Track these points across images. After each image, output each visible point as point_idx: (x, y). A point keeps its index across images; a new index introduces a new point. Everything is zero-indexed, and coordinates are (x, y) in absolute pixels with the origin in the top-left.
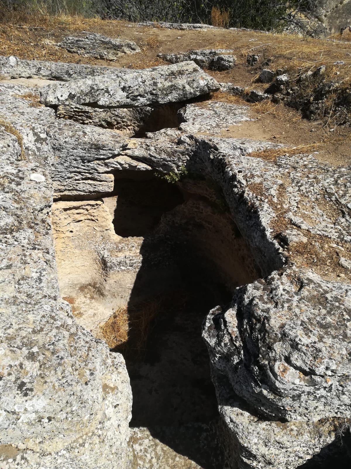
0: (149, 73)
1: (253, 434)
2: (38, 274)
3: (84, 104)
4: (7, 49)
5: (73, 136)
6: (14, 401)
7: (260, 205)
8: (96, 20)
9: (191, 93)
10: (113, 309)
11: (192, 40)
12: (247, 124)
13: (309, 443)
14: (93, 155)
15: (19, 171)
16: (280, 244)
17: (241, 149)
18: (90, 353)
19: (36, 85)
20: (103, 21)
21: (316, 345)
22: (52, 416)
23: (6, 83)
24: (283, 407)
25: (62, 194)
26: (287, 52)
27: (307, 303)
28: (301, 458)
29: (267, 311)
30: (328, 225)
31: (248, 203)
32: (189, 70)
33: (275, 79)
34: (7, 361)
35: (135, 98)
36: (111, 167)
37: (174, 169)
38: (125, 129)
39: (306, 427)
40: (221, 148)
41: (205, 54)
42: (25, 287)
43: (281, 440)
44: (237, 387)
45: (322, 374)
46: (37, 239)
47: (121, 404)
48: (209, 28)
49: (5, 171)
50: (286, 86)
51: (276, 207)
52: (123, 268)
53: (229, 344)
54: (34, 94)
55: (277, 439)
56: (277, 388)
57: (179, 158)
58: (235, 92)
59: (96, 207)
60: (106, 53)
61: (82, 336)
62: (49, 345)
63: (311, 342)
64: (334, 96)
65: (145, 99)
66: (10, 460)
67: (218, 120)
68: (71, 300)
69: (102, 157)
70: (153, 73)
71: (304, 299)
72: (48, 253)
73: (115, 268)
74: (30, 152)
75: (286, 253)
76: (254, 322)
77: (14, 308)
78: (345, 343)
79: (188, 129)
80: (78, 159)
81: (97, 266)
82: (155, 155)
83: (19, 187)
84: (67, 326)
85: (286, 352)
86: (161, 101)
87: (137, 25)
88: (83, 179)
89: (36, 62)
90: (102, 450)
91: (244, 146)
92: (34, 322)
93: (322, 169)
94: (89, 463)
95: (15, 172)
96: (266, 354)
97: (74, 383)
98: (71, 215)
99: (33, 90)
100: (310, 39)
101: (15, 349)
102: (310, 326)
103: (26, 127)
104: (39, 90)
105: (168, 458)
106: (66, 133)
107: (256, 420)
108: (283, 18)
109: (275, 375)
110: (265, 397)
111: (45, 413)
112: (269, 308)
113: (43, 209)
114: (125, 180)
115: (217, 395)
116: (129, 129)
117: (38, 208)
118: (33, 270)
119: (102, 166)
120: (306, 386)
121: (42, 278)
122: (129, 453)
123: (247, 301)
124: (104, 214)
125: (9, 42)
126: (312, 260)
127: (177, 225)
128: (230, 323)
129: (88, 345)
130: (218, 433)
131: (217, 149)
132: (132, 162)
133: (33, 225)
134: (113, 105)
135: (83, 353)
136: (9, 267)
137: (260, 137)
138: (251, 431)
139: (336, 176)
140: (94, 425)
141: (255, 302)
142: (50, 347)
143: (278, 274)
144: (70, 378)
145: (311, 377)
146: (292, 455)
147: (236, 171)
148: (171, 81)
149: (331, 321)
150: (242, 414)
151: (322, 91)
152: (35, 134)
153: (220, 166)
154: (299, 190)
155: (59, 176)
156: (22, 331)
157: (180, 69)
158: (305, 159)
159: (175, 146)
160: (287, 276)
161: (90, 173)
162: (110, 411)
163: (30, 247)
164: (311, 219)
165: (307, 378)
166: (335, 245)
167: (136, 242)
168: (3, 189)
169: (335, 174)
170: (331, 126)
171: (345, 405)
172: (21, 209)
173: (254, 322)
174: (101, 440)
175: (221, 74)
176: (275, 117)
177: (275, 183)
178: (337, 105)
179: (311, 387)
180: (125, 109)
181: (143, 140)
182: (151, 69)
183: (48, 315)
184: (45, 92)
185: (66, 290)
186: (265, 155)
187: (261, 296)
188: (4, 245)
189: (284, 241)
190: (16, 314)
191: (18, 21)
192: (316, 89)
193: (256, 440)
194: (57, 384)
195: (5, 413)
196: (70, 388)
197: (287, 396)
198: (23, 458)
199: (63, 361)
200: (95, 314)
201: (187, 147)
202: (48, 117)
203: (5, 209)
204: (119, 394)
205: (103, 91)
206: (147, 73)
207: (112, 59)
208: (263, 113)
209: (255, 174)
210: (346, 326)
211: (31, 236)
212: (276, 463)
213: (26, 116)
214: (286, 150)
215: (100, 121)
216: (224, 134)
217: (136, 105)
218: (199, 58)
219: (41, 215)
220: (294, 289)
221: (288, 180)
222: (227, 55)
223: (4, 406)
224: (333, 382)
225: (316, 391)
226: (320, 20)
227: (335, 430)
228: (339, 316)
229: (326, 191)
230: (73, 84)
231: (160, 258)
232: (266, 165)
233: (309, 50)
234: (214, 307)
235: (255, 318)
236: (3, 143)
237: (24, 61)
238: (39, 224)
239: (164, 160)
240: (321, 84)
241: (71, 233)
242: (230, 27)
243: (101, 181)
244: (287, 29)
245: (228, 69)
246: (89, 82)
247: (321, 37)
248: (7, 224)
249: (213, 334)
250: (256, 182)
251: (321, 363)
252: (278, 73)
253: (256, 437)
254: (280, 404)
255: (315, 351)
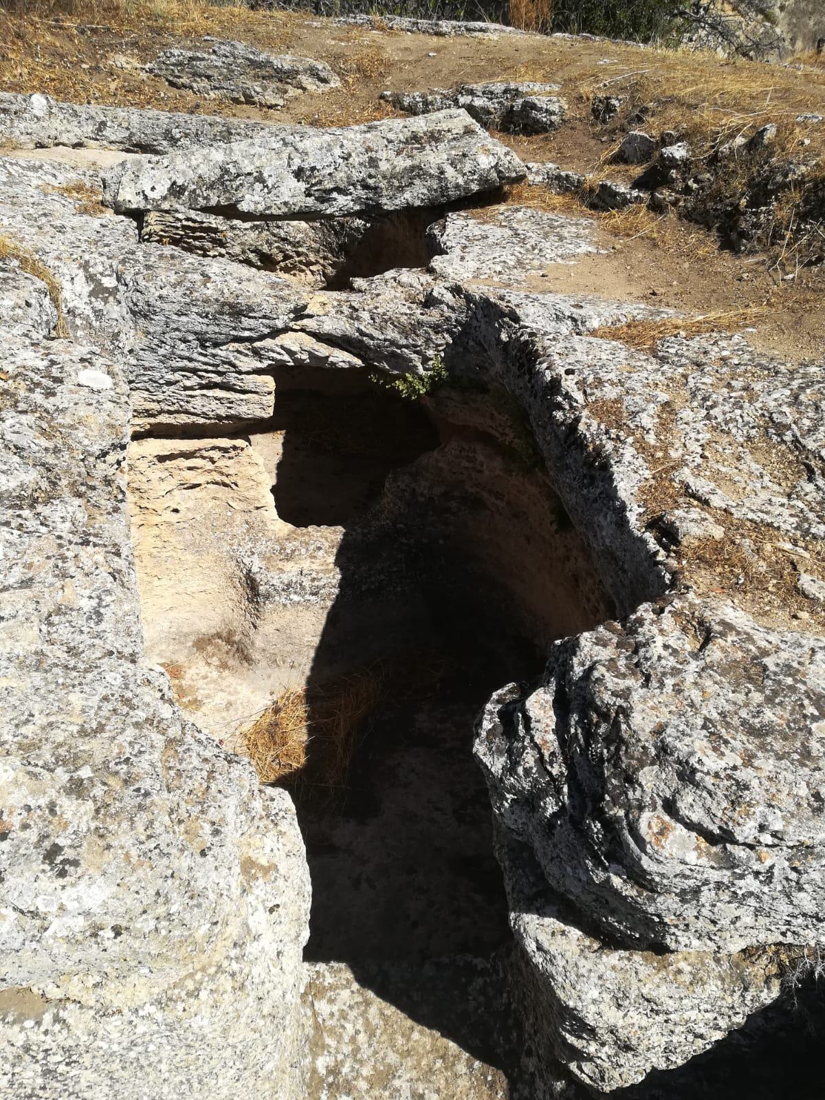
0: (358, 135)
1: (589, 978)
2: (94, 602)
3: (206, 210)
4: (26, 77)
5: (180, 283)
6: (33, 885)
7: (616, 450)
8: (236, 10)
9: (457, 186)
10: (272, 693)
11: (462, 61)
12: (589, 260)
13: (719, 1003)
14: (225, 330)
15: (53, 363)
16: (660, 542)
17: (574, 320)
18: (213, 786)
19: (94, 164)
20: (252, 13)
21: (738, 773)
22: (124, 924)
23: (23, 157)
24: (659, 916)
25: (152, 420)
26: (689, 90)
27: (718, 678)
28: (701, 1036)
29: (626, 694)
30: (774, 499)
31: (587, 446)
32: (454, 132)
33: (657, 154)
34: (18, 798)
35: (325, 197)
36: (269, 358)
37: (415, 366)
38: (303, 271)
39: (713, 964)
40: (527, 316)
41: (492, 93)
42: (63, 632)
43: (654, 994)
44: (551, 869)
45: (750, 841)
46: (92, 522)
47: (285, 904)
48: (502, 31)
49: (19, 364)
50: (684, 172)
51: (653, 456)
52: (296, 598)
53: (534, 770)
54: (88, 185)
55: (645, 991)
56: (645, 871)
57: (428, 340)
58: (563, 184)
59: (233, 453)
60: (259, 89)
61: (195, 747)
62: (116, 764)
63: (724, 765)
64: (796, 196)
65: (349, 197)
66: (29, 1024)
67: (522, 250)
68: (175, 671)
69: (247, 334)
70: (368, 135)
71: (711, 668)
72: (118, 554)
73: (277, 598)
74: (78, 321)
75: (673, 563)
76: (595, 720)
77: (37, 678)
78: (806, 770)
79: (450, 270)
80: (190, 338)
81: (236, 593)
82: (370, 330)
83: (51, 399)
84: (159, 722)
85: (667, 790)
86: (388, 204)
87: (334, 23)
88: (202, 387)
89: (94, 109)
90: (239, 1006)
91: (581, 312)
92: (83, 711)
93: (763, 368)
94: (210, 1036)
95: (42, 365)
96: (621, 794)
97: (174, 851)
98: (176, 472)
99: (88, 174)
100: (741, 61)
101: (38, 770)
102: (723, 731)
103: (69, 261)
104: (102, 174)
105: (394, 1032)
106: (163, 277)
107: (596, 946)
108: (682, 14)
109: (641, 842)
110: (617, 893)
111: (107, 917)
112: (628, 689)
113: (107, 453)
114: (302, 389)
115: (508, 889)
116: (312, 272)
117: (96, 449)
118: (83, 592)
119: (246, 355)
120: (712, 868)
121: (102, 610)
122: (304, 1020)
123: (578, 671)
124: (252, 471)
125: (30, 60)
126: (734, 580)
127: (422, 499)
128: (538, 721)
129: (207, 767)
130: (509, 977)
131: (516, 319)
132: (316, 347)
133: (83, 489)
134: (275, 211)
135: (197, 784)
136: (26, 583)
137: (620, 292)
138: (583, 971)
139: (795, 384)
140: (220, 952)
141: (596, 674)
142: (119, 767)
143: (654, 611)
144: (164, 839)
145: (725, 848)
146: (678, 1029)
147: (562, 371)
148: (411, 157)
149: (775, 719)
150: (563, 933)
151: (766, 185)
152: (90, 278)
153: (524, 360)
154: (708, 417)
155: (146, 378)
156: (55, 731)
157: (432, 127)
158: (723, 343)
159: (419, 311)
160: (675, 614)
161: (220, 373)
162: (260, 920)
163: (76, 539)
164: (735, 483)
165: (714, 849)
166: (788, 546)
167: (325, 540)
168: (15, 405)
169: (793, 379)
170: (788, 269)
171: (804, 915)
172: (56, 451)
173: (595, 720)
174: (237, 985)
175: (530, 142)
176: (655, 246)
177: (651, 399)
178: (803, 217)
179: (725, 872)
180: (303, 225)
181: (343, 296)
182: (363, 128)
183: (116, 696)
184: (115, 180)
185: (164, 647)
186: (630, 335)
187: (612, 660)
188: (16, 532)
189: (668, 534)
190: (42, 691)
191: (51, 11)
192: (753, 179)
193: (594, 993)
194: (134, 852)
195: (14, 915)
196: (165, 861)
197: (668, 892)
198: (57, 1019)
199: (148, 800)
200: (230, 704)
201: (448, 313)
202: (121, 238)
203: (18, 450)
204: (280, 882)
205: (251, 179)
206: (354, 137)
207: (273, 102)
208: (628, 235)
209: (606, 379)
210: (810, 732)
211: (79, 516)
212: (641, 1048)
213: (70, 236)
214: (680, 322)
215: (244, 252)
216: (534, 283)
217: (328, 212)
218: (478, 102)
219: (103, 466)
220: (689, 645)
221: (682, 392)
222: (545, 96)
223: (12, 898)
224: (776, 860)
225: (736, 882)
226: (768, 17)
227: (781, 974)
228: (793, 710)
229: (771, 418)
230: (179, 160)
231: (383, 577)
232: (632, 357)
233: (739, 86)
234: (501, 686)
235: (597, 709)
236: (14, 298)
237: (65, 105)
238: (96, 485)
239: (393, 343)
240: (766, 167)
241: (174, 514)
242: (553, 31)
243: (244, 392)
244: (691, 40)
245: (547, 131)
246: (218, 156)
247: (770, 58)
248: (22, 485)
249: (498, 747)
250: (607, 397)
251: (748, 815)
252: (666, 140)
253: (596, 985)
254: (651, 910)
255: (734, 788)
